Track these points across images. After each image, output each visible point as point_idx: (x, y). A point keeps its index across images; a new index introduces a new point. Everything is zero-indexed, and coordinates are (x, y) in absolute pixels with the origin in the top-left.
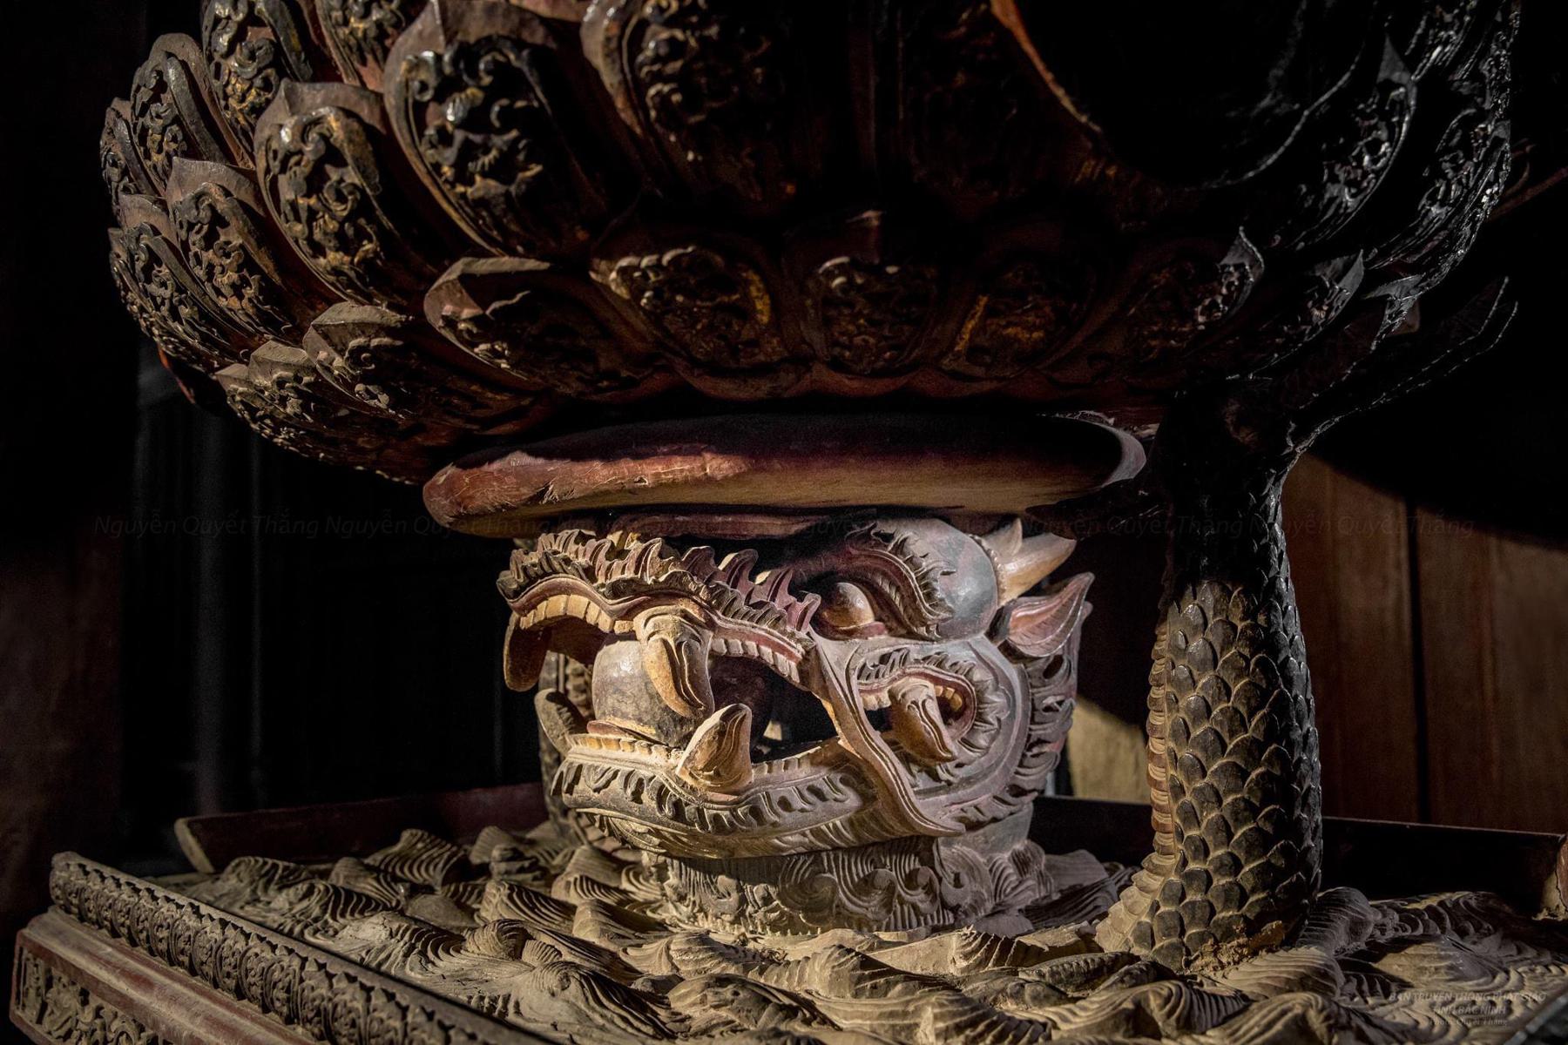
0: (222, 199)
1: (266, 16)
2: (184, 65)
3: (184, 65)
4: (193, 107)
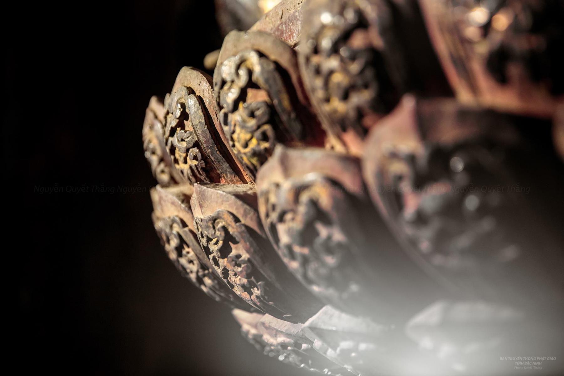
0: (233, 224)
1: (261, 81)
2: (201, 100)
3: (201, 100)
4: (209, 136)
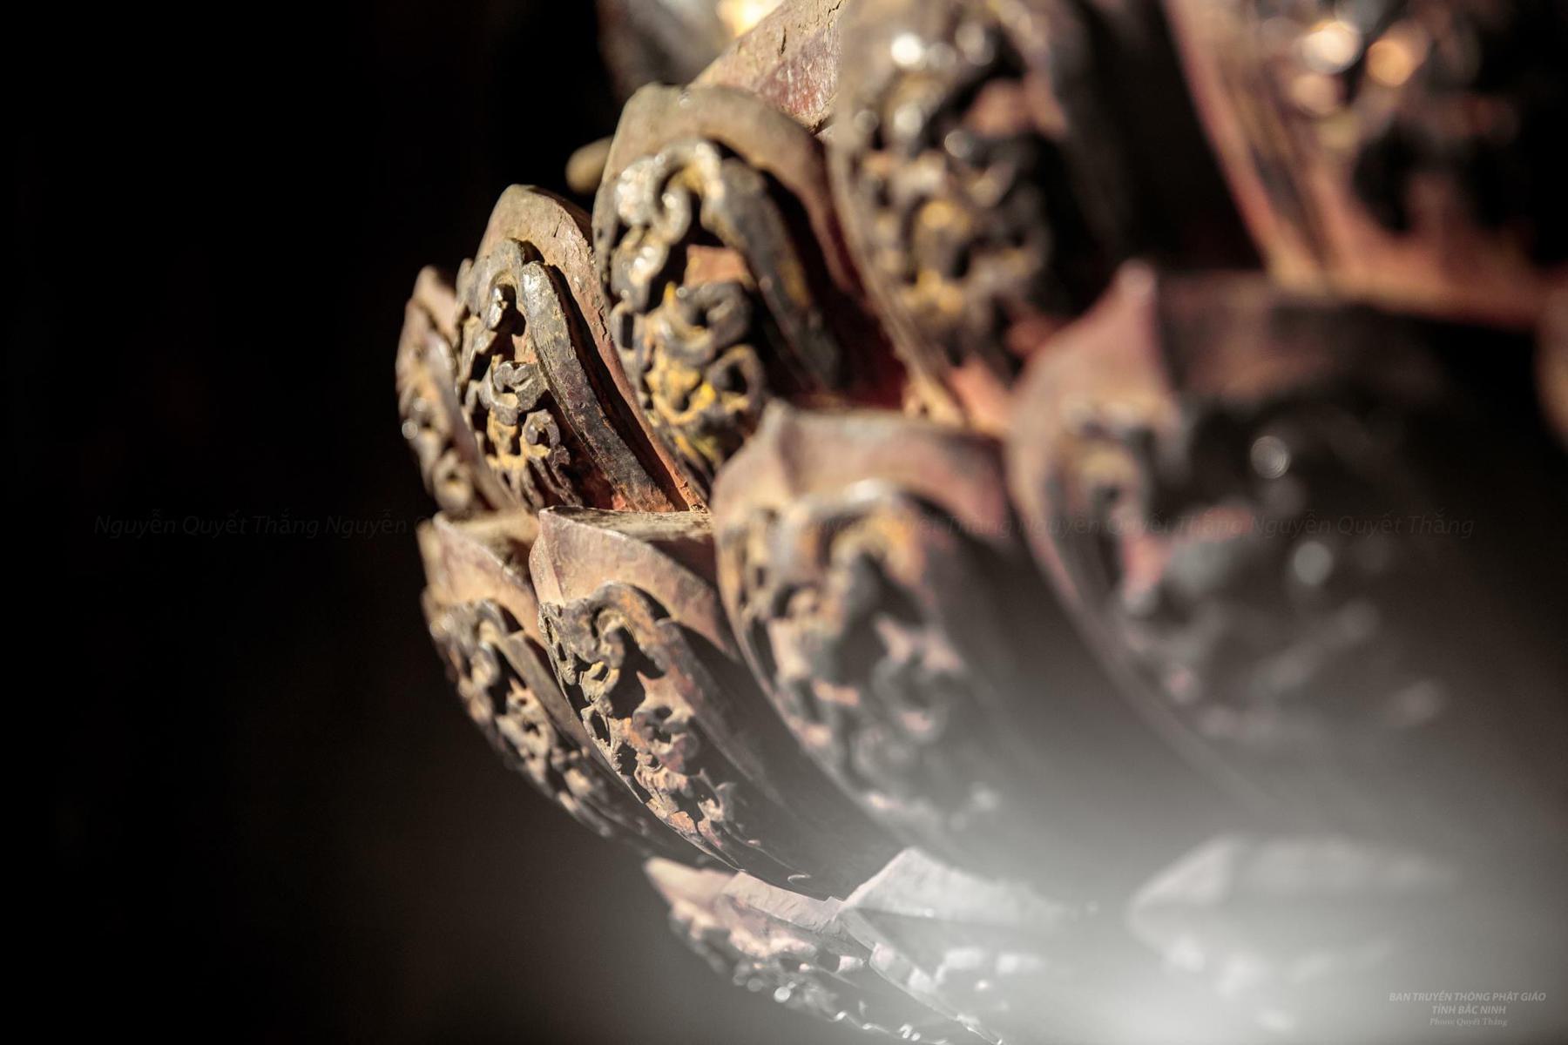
0: (648, 622)
1: (725, 226)
2: (557, 279)
3: (557, 279)
4: (580, 377)
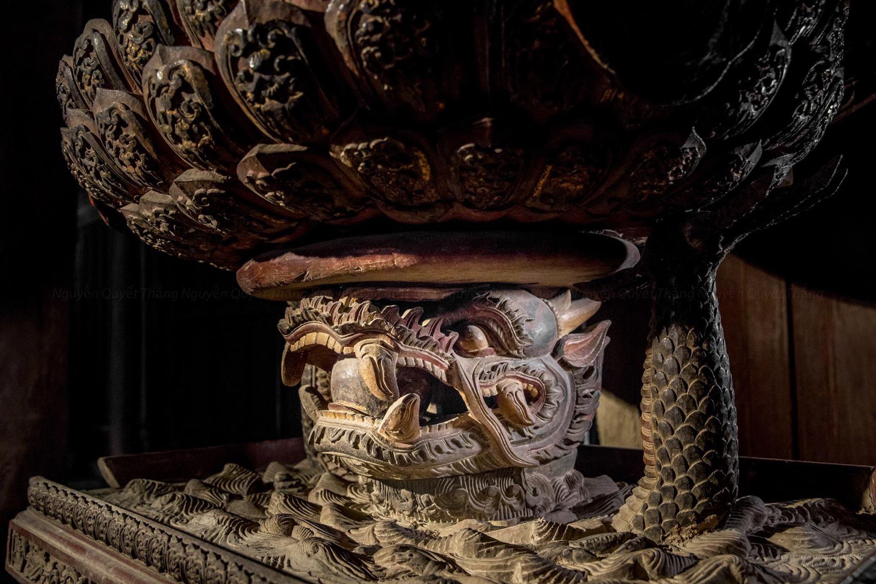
0: (124, 111)
1: (148, 9)
2: (103, 36)
3: (103, 36)
4: (108, 60)
